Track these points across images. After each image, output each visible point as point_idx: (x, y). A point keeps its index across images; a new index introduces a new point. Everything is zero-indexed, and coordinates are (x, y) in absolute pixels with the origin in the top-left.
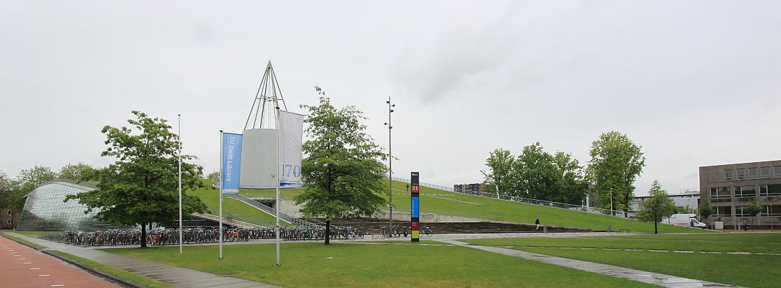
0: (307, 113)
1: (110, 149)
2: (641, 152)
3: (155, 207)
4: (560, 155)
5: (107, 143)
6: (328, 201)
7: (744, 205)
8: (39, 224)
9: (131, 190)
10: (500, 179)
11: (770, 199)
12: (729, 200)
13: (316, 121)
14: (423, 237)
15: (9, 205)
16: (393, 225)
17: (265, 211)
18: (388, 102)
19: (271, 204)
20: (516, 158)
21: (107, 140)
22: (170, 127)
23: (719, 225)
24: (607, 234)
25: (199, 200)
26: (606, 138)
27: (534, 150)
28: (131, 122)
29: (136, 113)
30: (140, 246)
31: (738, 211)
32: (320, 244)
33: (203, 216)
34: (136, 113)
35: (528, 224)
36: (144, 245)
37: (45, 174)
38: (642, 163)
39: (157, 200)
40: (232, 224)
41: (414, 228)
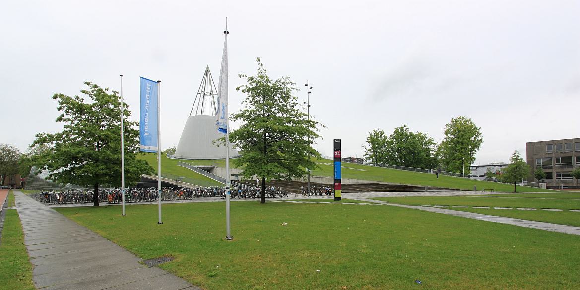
0: (245, 83)
1: (63, 116)
2: (480, 132)
3: (102, 169)
4: (420, 134)
5: (59, 109)
6: (266, 164)
7: (561, 171)
8: (40, 185)
9: (79, 152)
10: (376, 152)
11: (562, 167)
12: (551, 167)
13: (254, 92)
14: (345, 196)
15: (21, 172)
16: (311, 185)
17: (205, 175)
18: (306, 85)
19: (209, 170)
20: (389, 137)
21: (59, 106)
22: (120, 98)
23: (544, 186)
24: (473, 193)
25: (147, 163)
26: (456, 122)
27: (403, 131)
28: (84, 92)
29: (88, 84)
30: (93, 205)
31: (558, 176)
32: (256, 203)
33: (151, 178)
34: (88, 84)
35: (409, 185)
36: (96, 204)
37: (46, 150)
38: (481, 140)
39: (106, 163)
40: (180, 185)
41: (336, 189)
